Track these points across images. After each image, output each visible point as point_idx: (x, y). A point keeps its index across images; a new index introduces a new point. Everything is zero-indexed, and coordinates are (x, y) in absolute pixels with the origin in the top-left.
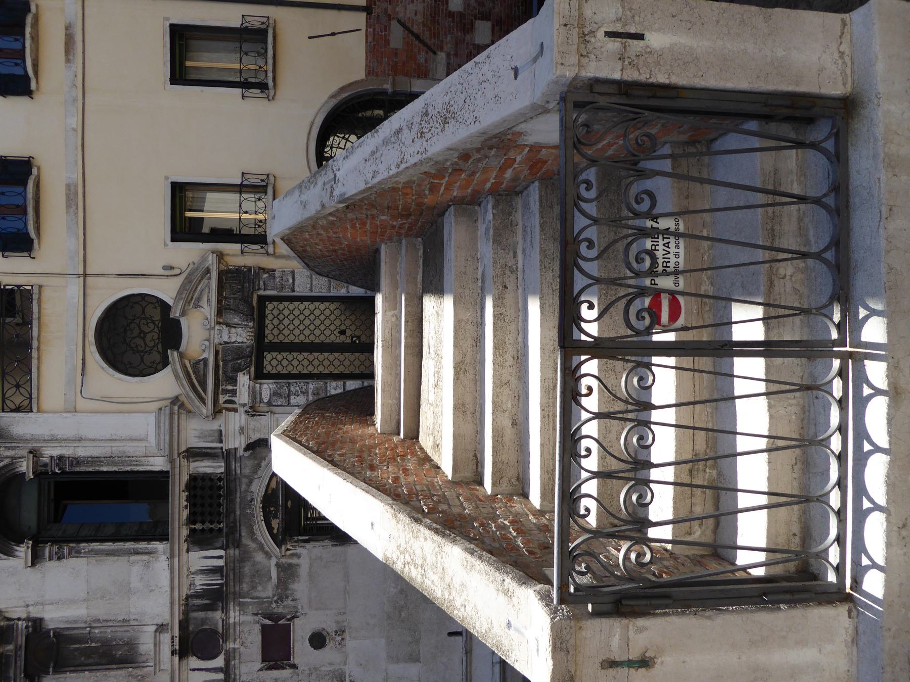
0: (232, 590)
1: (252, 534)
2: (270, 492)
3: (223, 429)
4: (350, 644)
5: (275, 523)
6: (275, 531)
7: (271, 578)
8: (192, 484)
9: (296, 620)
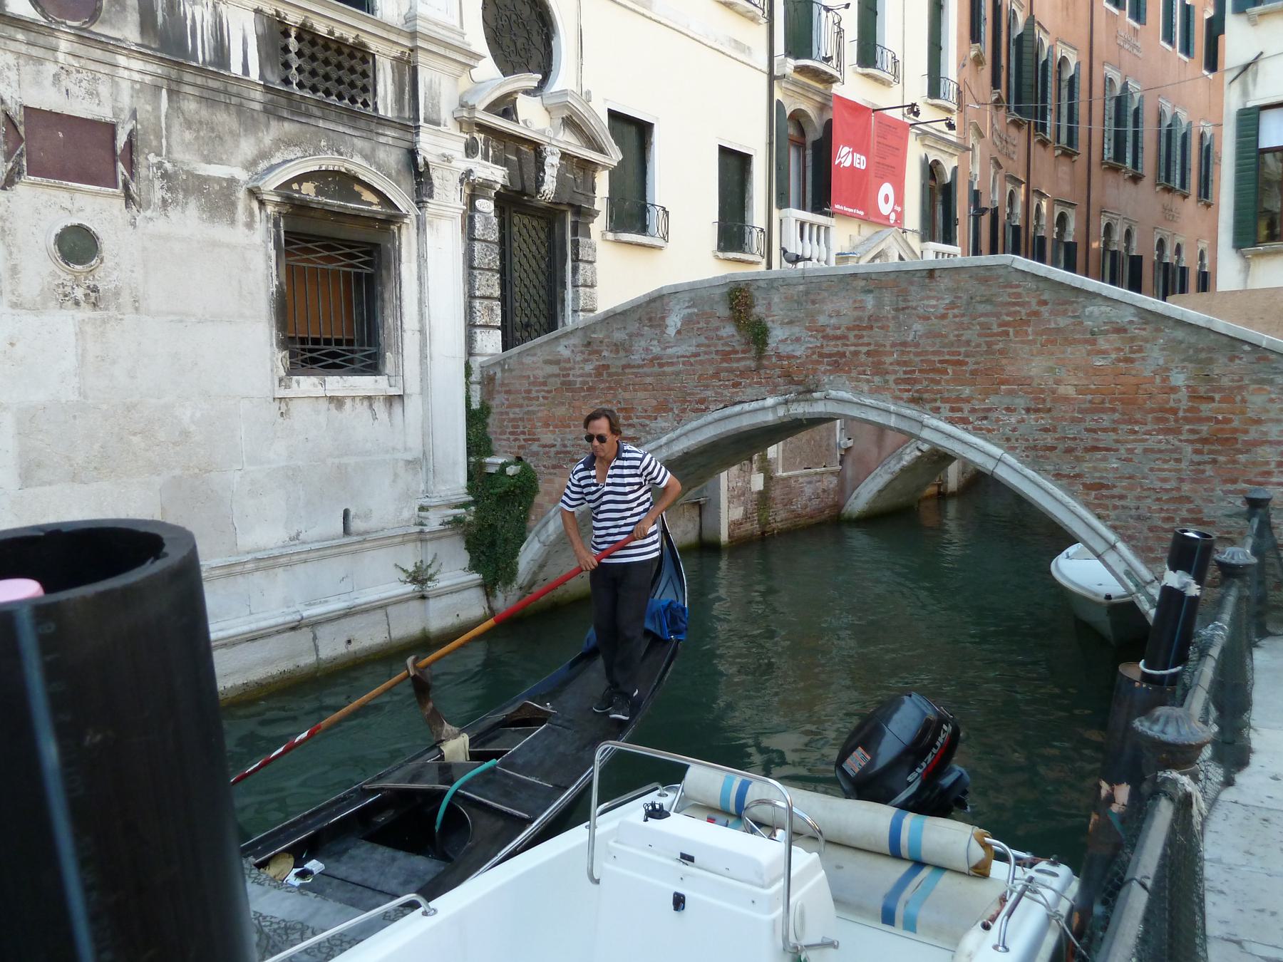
0: (188, 77)
1: (289, 142)
2: (357, 188)
3: (442, 128)
4: (66, 321)
5: (308, 189)
7: (209, 163)
8: (359, 55)
9: (121, 202)
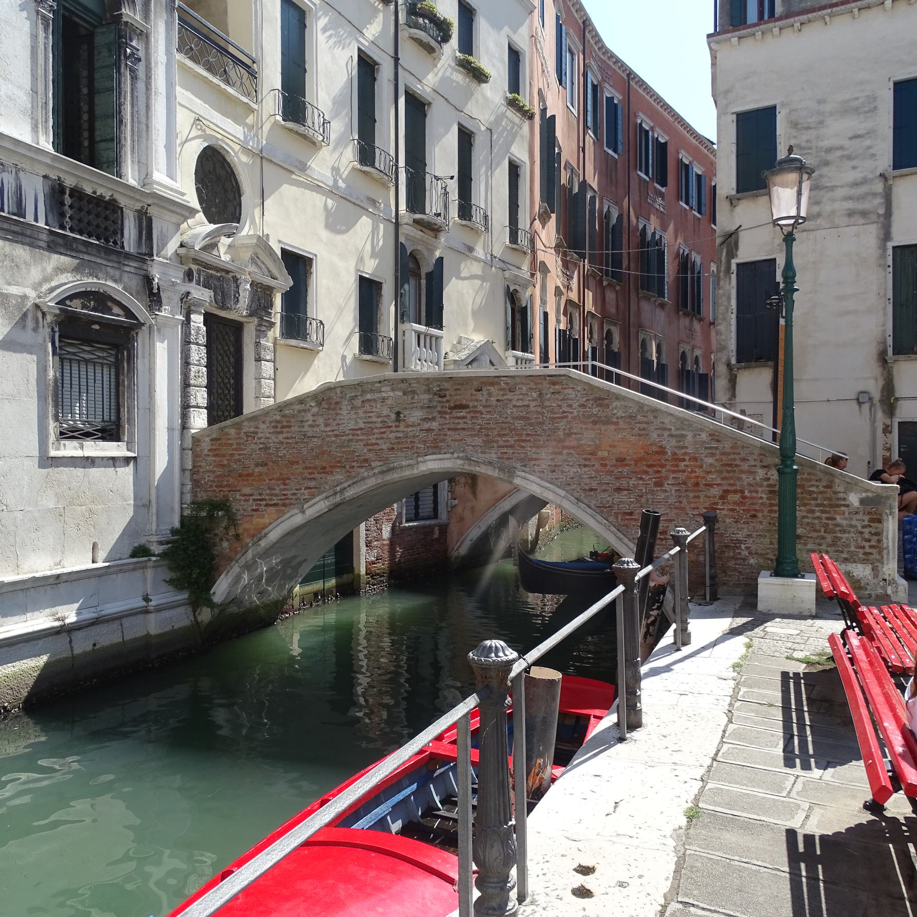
2: (109, 304)
6: (68, 302)
7: (9, 284)
